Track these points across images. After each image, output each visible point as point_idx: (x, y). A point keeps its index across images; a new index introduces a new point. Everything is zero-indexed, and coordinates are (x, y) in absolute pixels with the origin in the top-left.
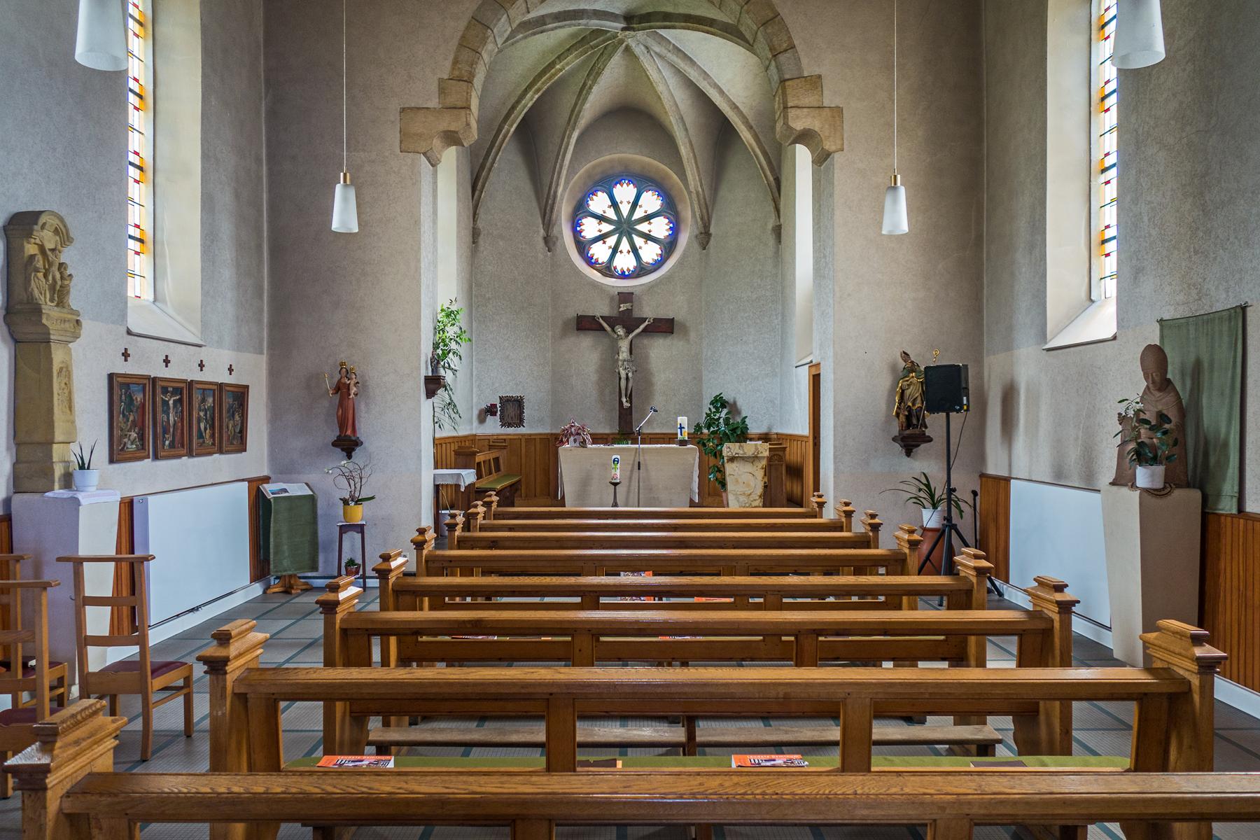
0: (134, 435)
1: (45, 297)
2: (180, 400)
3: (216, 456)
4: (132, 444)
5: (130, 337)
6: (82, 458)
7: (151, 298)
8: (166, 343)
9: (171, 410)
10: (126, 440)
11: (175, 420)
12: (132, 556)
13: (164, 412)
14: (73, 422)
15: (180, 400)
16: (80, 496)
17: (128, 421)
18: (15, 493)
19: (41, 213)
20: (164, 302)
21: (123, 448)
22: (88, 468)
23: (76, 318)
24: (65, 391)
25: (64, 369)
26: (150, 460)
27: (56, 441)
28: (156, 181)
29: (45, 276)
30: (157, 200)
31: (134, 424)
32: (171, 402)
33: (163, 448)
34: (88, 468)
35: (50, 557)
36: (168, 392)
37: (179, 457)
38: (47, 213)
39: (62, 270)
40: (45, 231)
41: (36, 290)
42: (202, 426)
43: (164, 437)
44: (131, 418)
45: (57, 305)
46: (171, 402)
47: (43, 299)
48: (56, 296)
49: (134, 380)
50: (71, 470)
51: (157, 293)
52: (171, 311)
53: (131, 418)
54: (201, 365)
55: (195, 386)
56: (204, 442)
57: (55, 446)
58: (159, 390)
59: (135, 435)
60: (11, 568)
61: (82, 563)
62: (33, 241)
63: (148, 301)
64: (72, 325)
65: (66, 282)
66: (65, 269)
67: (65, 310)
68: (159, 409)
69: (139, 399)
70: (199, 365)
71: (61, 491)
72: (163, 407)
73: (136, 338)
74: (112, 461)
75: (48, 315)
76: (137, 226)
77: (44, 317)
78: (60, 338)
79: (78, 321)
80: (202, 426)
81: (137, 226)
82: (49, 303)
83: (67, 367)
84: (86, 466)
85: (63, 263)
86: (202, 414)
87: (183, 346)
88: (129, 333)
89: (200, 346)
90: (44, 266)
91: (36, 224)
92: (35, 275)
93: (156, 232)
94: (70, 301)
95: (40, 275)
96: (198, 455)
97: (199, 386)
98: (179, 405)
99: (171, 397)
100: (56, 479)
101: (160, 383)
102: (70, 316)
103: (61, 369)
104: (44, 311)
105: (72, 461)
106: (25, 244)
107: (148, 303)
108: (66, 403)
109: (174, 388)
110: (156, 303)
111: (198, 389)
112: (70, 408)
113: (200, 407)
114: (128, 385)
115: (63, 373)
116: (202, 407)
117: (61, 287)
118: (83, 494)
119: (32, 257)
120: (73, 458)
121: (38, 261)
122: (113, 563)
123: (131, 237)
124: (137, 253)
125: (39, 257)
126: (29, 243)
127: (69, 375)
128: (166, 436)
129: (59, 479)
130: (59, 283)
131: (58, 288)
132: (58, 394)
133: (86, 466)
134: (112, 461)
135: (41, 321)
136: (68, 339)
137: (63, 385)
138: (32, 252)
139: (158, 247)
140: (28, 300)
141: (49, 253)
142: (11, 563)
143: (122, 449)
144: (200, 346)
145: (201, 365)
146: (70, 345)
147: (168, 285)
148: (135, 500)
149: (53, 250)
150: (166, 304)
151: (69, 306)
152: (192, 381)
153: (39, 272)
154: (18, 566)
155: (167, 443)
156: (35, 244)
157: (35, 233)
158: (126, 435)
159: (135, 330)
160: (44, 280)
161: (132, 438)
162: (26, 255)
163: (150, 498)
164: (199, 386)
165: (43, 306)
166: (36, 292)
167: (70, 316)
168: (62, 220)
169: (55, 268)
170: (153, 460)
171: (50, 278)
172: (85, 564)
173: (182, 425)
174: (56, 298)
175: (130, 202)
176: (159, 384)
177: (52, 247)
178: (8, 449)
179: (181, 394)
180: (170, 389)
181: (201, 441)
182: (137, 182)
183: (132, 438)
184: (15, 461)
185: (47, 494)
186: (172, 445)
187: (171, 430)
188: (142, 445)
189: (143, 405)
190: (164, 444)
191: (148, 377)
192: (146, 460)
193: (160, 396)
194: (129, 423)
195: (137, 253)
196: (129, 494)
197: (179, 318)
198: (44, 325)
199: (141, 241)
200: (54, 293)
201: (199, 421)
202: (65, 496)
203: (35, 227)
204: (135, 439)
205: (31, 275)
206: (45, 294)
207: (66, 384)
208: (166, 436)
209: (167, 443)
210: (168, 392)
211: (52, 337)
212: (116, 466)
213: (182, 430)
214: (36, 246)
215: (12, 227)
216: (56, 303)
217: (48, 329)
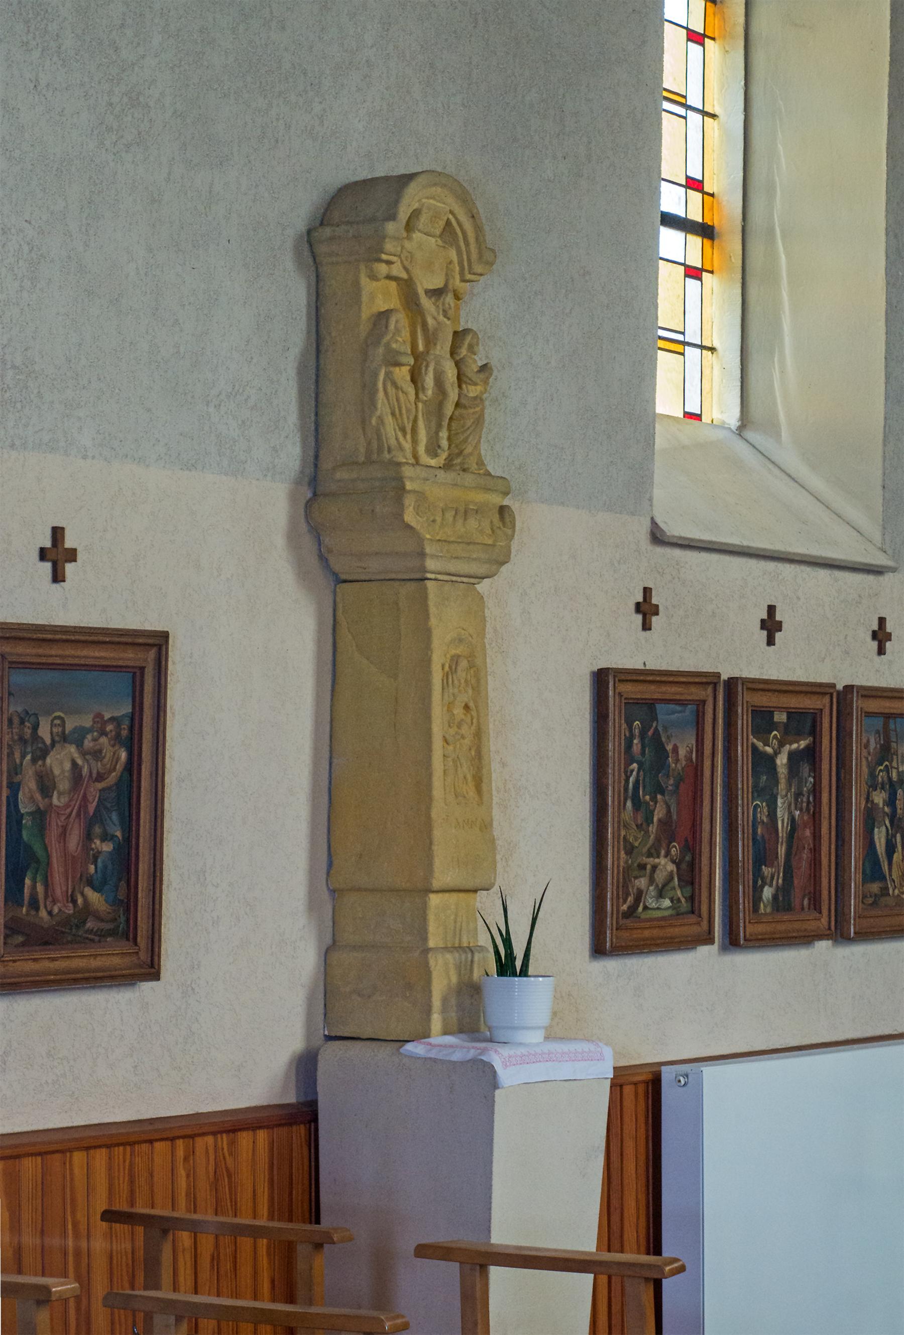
0: (666, 866)
1: (415, 442)
2: (811, 755)
3: (823, 945)
4: (660, 895)
5: (660, 550)
6: (507, 941)
7: (731, 416)
8: (771, 566)
9: (782, 785)
10: (642, 883)
11: (792, 820)
12: (316, 1227)
13: (758, 791)
14: (486, 826)
15: (811, 755)
16: (497, 1058)
17: (649, 820)
18: (329, 1038)
19: (407, 179)
20: (772, 429)
21: (633, 909)
22: (524, 973)
23: (496, 500)
24: (465, 730)
25: (464, 664)
26: (715, 947)
27: (436, 884)
28: (755, 30)
29: (415, 378)
30: (757, 90)
31: (668, 829)
32: (782, 760)
33: (756, 909)
34: (524, 973)
35: (407, 1244)
36: (773, 726)
37: (806, 939)
38: (420, 179)
39: (463, 352)
40: (417, 235)
41: (389, 420)
42: (880, 837)
43: (757, 873)
44: (659, 813)
45: (447, 466)
46: (782, 760)
47: (407, 445)
48: (444, 434)
49: (671, 691)
50: (477, 974)
51: (753, 401)
52: (790, 459)
53: (659, 813)
54: (881, 636)
55: (857, 703)
56: (884, 891)
57: (434, 900)
58: (743, 721)
59: (671, 867)
60: (301, 1265)
61: (484, 1269)
62: (383, 269)
63: (722, 426)
64: (486, 524)
65: (472, 391)
66: (471, 349)
67: (469, 479)
68: (744, 781)
69: (682, 752)
70: (875, 635)
71: (449, 1039)
72: (756, 773)
73: (677, 553)
74: (599, 950)
75: (421, 495)
76: (694, 184)
77: (409, 502)
78: (452, 567)
79: (503, 510)
80: (880, 837)
81: (694, 184)
82: (425, 459)
83: (471, 657)
84: (518, 964)
85: (466, 331)
86: (879, 798)
87: (823, 573)
88: (657, 537)
89: (876, 571)
90: (414, 346)
91: (393, 217)
92: (388, 374)
93: (752, 195)
94: (484, 448)
95: (402, 374)
96: (866, 935)
97: (873, 706)
98: (805, 769)
99: (782, 744)
100: (436, 1002)
101: (748, 697)
102: (480, 497)
103: (456, 659)
104: (409, 486)
105: (482, 949)
106: (364, 280)
107: (721, 434)
108: (466, 769)
109: (792, 714)
110: (749, 434)
111: (869, 714)
112: (479, 781)
113: (872, 775)
114: (650, 705)
115: (461, 674)
116: (881, 777)
117: (458, 405)
118: (505, 1051)
119: (383, 316)
120: (484, 940)
121: (398, 331)
122: (455, 1267)
123: (669, 220)
124: (693, 273)
125: (400, 321)
126: (373, 277)
127: (477, 684)
128: (766, 871)
129: (445, 1001)
130: (453, 395)
131: (449, 409)
132: (446, 740)
133: (518, 964)
134: (599, 950)
135: (399, 515)
136: (481, 570)
137: (458, 711)
138: (382, 305)
139: (757, 250)
140: (369, 452)
141: (426, 303)
142: (302, 1250)
143: (631, 913)
144: (876, 571)
145: (881, 636)
146: (483, 587)
147: (783, 372)
148: (667, 1074)
149: (436, 293)
150: (778, 435)
151: (481, 463)
152: (849, 688)
153: (398, 364)
154: (320, 1261)
155: (768, 893)
156: (389, 277)
157: (389, 246)
158: (642, 867)
159: (674, 528)
160: (411, 390)
161: (660, 877)
162: (366, 313)
163: (709, 1072)
164: (873, 706)
165: (407, 471)
166: (390, 428)
167: (480, 497)
168: (464, 198)
169: (443, 348)
170: (724, 949)
171: (429, 381)
172: (496, 1273)
173: (816, 836)
174: (444, 443)
175: (666, 105)
176: (745, 700)
177: (437, 282)
178: (312, 905)
179: (814, 731)
180: (780, 717)
181: (875, 887)
182: (695, 37)
183: (660, 877)
184: (328, 940)
185: (409, 1047)
186: (782, 903)
187: (782, 850)
188: (691, 899)
189: (696, 769)
190: (757, 899)
191: (710, 680)
192: (704, 950)
193: (746, 739)
194: (653, 829)
195: (693, 273)
196: (647, 1055)
197: (816, 482)
198: (409, 527)
199: (705, 231)
200: (439, 426)
201: (870, 819)
202: (457, 1056)
203: (391, 227)
204: (670, 878)
205: (375, 375)
206: (414, 430)
207: (467, 707)
208: (766, 871)
209: (768, 893)
210: (773, 726)
211: (430, 564)
212: (611, 965)
213: (816, 850)
214: (393, 285)
215: (327, 231)
216: (444, 455)
217: (420, 540)
